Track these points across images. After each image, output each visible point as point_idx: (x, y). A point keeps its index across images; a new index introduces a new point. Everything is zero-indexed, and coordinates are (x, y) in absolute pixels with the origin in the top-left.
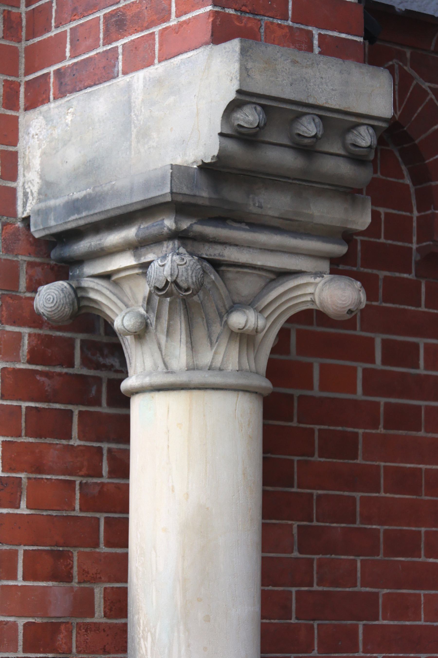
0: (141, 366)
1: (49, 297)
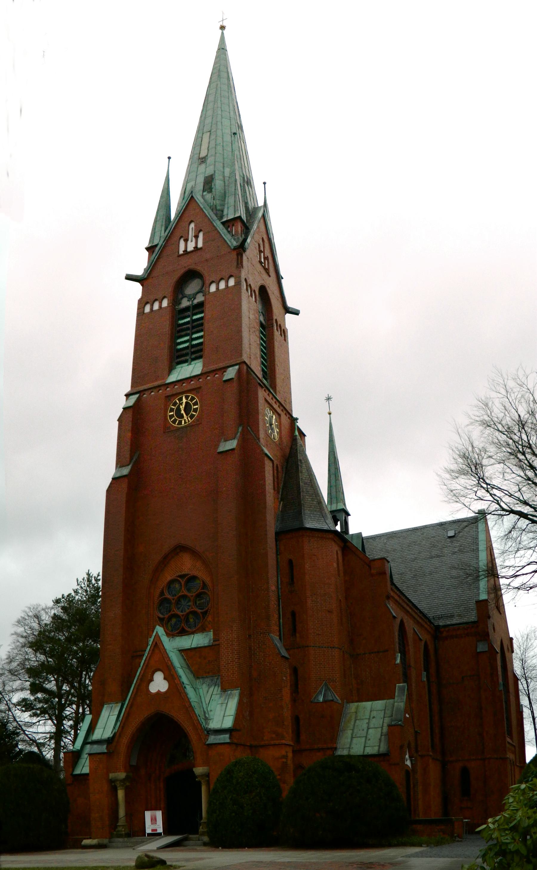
0: (119, 788)
1: (113, 784)
